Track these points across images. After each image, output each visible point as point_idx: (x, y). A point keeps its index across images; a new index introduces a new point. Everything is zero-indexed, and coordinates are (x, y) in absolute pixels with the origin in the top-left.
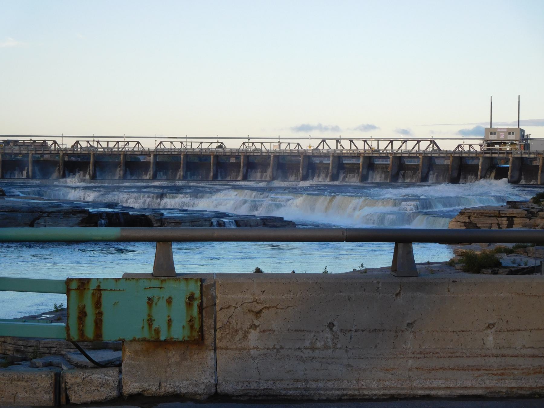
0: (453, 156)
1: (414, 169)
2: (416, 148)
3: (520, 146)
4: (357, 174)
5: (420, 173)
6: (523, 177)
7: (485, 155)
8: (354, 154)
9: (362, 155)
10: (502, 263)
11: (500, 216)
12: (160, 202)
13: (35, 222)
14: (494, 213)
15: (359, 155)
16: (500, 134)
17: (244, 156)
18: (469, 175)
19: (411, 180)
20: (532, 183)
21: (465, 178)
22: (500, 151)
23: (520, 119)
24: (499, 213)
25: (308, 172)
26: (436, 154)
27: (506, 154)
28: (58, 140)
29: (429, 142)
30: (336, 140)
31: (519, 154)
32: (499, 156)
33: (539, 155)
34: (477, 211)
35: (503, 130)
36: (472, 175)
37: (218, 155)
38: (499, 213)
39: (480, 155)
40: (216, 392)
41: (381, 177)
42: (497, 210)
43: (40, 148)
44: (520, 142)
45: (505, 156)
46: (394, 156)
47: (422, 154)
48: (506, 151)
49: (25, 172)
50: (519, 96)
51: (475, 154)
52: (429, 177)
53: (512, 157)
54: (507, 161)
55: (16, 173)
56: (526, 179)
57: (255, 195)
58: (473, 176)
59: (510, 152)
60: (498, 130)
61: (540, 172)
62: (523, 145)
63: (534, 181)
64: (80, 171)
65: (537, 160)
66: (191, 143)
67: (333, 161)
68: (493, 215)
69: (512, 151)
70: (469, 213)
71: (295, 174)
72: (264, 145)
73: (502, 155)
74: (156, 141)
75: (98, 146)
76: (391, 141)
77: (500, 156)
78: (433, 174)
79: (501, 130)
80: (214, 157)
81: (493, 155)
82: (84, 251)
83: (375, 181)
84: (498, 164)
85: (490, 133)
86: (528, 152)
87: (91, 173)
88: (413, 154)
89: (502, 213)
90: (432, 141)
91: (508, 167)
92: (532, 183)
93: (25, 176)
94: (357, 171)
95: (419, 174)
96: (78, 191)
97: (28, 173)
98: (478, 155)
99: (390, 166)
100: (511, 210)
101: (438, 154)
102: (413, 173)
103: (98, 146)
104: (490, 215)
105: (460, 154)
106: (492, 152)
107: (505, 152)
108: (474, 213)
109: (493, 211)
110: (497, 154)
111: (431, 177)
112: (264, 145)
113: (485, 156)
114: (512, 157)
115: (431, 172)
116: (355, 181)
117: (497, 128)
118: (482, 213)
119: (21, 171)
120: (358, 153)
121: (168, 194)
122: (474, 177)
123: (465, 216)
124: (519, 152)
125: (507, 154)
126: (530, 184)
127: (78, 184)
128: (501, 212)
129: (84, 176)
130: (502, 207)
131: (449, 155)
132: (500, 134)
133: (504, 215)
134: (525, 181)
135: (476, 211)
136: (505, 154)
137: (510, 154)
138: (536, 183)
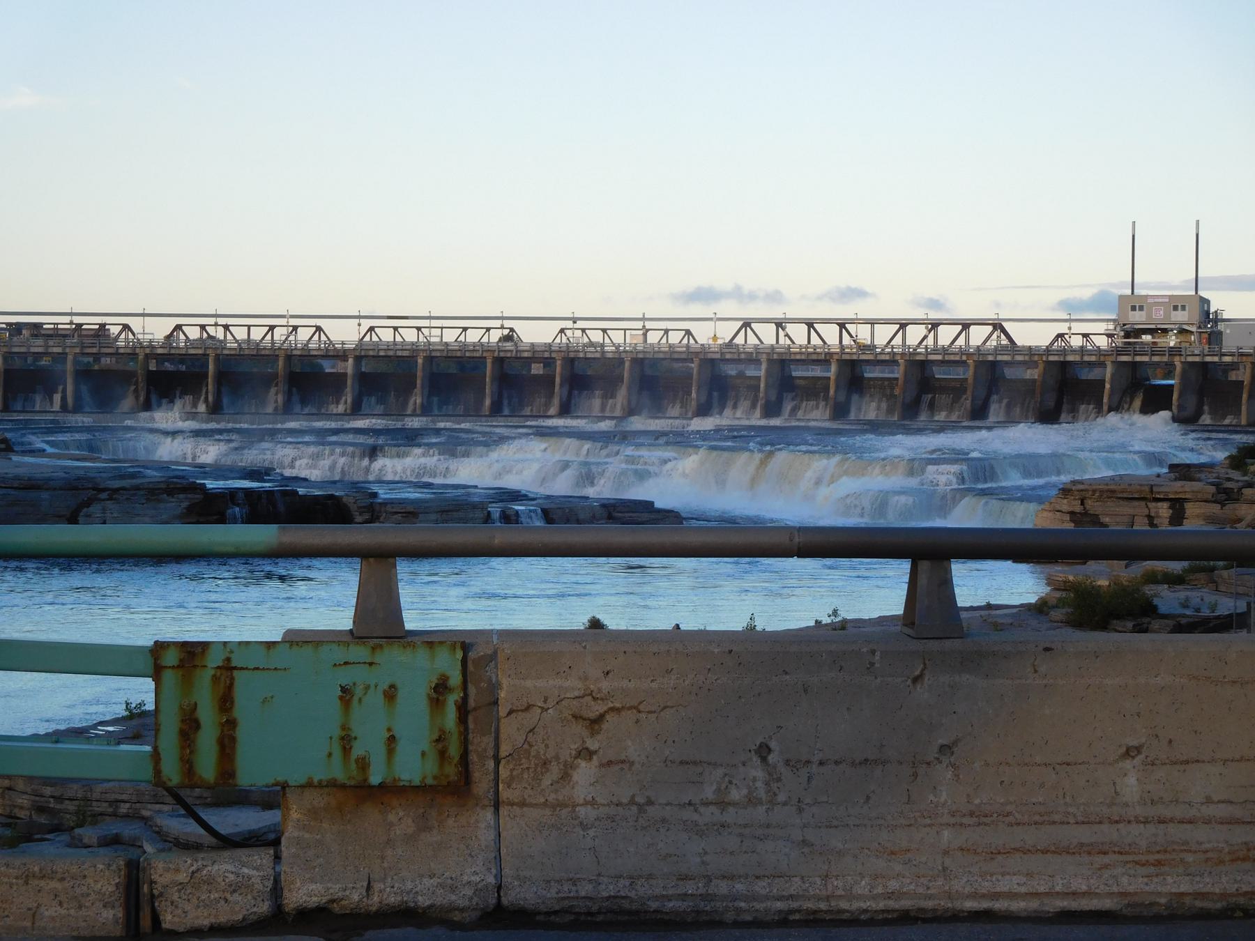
0: (1044, 359)
1: (956, 390)
2: (961, 341)
3: (1200, 336)
4: (823, 400)
5: (970, 399)
6: (1206, 408)
7: (1118, 357)
8: (816, 355)
9: (836, 357)
10: (1159, 607)
11: (1153, 498)
12: (370, 465)
13: (81, 511)
14: (1140, 492)
15: (828, 358)
16: (1154, 308)
17: (564, 359)
18: (1083, 404)
19: (947, 416)
20: (1227, 422)
21: (1074, 411)
22: (1153, 349)
23: (1199, 275)
24: (1152, 492)
25: (710, 396)
26: (1006, 356)
27: (1167, 355)
28: (135, 323)
29: (990, 328)
30: (776, 324)
31: (1197, 355)
32: (1151, 359)
33: (1244, 358)
34: (1100, 487)
35: (1160, 300)
36: (1089, 404)
37: (502, 358)
38: (1152, 492)
39: (1107, 357)
40: (499, 904)
41: (878, 408)
42: (1147, 485)
43: (92, 341)
44: (1200, 327)
45: (1165, 359)
46: (910, 360)
47: (974, 356)
48: (1166, 349)
49: (57, 398)
50: (1198, 222)
51: (1096, 355)
52: (990, 408)
53: (1182, 362)
54: (1169, 371)
55: (38, 398)
56: (1213, 413)
57: (588, 449)
58: (1091, 406)
59: (1176, 351)
60: (1150, 301)
61: (1245, 396)
62: (1206, 336)
63: (1233, 416)
64: (184, 393)
65: (1239, 369)
66: (440, 329)
67: (767, 371)
68: (1137, 496)
69: (1181, 348)
70: (1082, 490)
71: (682, 402)
72: (608, 335)
73: (1158, 357)
74: (359, 325)
75: (225, 336)
76: (903, 326)
77: (1153, 360)
78: (1000, 401)
79: (1156, 300)
80: (493, 363)
81: (1138, 359)
82: (193, 578)
83: (864, 417)
84: (1148, 379)
85: (1130, 307)
86: (1217, 351)
87: (210, 398)
88: (953, 355)
89: (1158, 490)
90: (998, 326)
91: (1172, 386)
92: (1227, 422)
93: (57, 407)
94: (824, 395)
95: (968, 401)
96: (179, 439)
97: (64, 399)
98: (1102, 359)
99: (900, 382)
100: (1179, 485)
101: (1010, 354)
102: (953, 398)
103: (225, 336)
104: (1131, 496)
105: (1061, 355)
106: (1135, 351)
107: (1165, 351)
108: (1094, 491)
109: (1138, 487)
110: (1146, 355)
111: (993, 407)
112: (608, 335)
113: (1118, 360)
114: (1182, 362)
115: (995, 397)
116: (818, 418)
117: (1147, 296)
118: (1113, 491)
119: (49, 394)
120: (826, 354)
121: (386, 448)
122: (1093, 409)
123: (1072, 497)
124: (1197, 350)
125: (1170, 355)
126: (1223, 425)
127: (181, 425)
128: (1155, 489)
129: (195, 405)
130: (1158, 479)
131: (1036, 358)
132: (1154, 308)
133: (1162, 497)
134: (1211, 419)
135: (1098, 487)
136: (1165, 355)
137: (1176, 355)
138: (1237, 422)
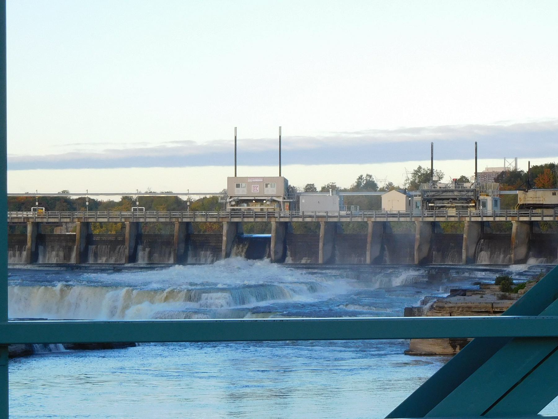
0: (180, 220)
1: (168, 242)
3: (284, 203)
4: (18, 251)
5: (128, 248)
6: (289, 253)
7: (62, 219)
8: (17, 219)
9: (31, 220)
11: (493, 311)
14: (486, 307)
15: (26, 221)
16: (252, 186)
20: (303, 261)
21: (196, 255)
23: (430, 161)
24: (493, 308)
25: (383, 249)
26: (153, 219)
27: (266, 217)
31: (287, 217)
32: (387, 220)
34: (463, 305)
35: (257, 180)
37: (38, 223)
38: (493, 308)
39: (224, 219)
41: (57, 255)
44: (284, 199)
45: (265, 220)
46: (85, 222)
47: (131, 219)
48: (266, 213)
50: (280, 128)
51: (216, 217)
53: (276, 222)
54: (265, 228)
56: (294, 255)
58: (208, 253)
59: (271, 215)
61: (321, 245)
63: (307, 258)
65: (62, 226)
68: (483, 310)
69: (274, 213)
71: (504, 251)
73: (260, 219)
78: (144, 250)
79: (254, 180)
80: (130, 227)
81: (533, 219)
83: (48, 261)
85: (236, 185)
86: (156, 215)
88: (115, 219)
91: (269, 239)
92: (303, 261)
95: (126, 250)
98: (220, 220)
99: (78, 237)
100: (509, 303)
102: (110, 248)
105: (192, 217)
106: (243, 215)
108: (459, 308)
109: (485, 305)
111: (140, 254)
114: (276, 222)
115: (140, 247)
116: (16, 263)
117: (247, 177)
118: (470, 308)
122: (210, 254)
123: (445, 312)
124: (285, 214)
125: (268, 217)
126: (97, 264)
127: (525, 279)
128: (495, 305)
130: (482, 299)
131: (174, 220)
132: (252, 186)
136: (265, 217)
138: (310, 262)
